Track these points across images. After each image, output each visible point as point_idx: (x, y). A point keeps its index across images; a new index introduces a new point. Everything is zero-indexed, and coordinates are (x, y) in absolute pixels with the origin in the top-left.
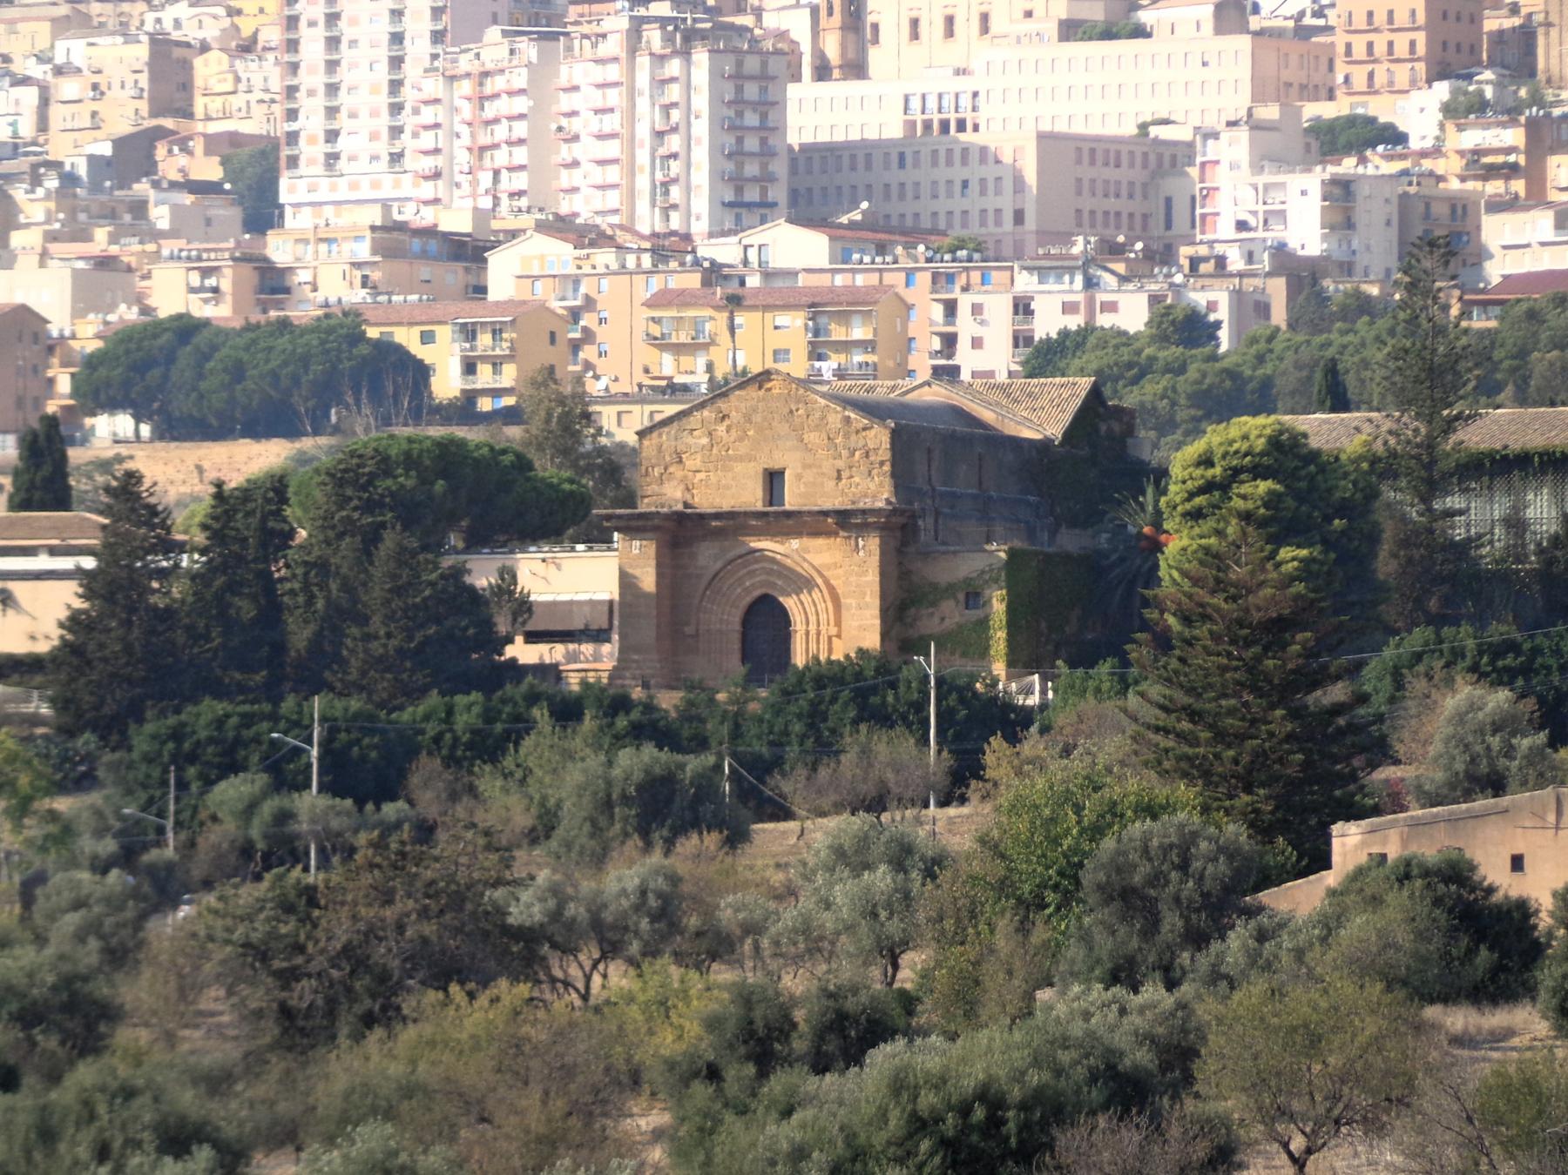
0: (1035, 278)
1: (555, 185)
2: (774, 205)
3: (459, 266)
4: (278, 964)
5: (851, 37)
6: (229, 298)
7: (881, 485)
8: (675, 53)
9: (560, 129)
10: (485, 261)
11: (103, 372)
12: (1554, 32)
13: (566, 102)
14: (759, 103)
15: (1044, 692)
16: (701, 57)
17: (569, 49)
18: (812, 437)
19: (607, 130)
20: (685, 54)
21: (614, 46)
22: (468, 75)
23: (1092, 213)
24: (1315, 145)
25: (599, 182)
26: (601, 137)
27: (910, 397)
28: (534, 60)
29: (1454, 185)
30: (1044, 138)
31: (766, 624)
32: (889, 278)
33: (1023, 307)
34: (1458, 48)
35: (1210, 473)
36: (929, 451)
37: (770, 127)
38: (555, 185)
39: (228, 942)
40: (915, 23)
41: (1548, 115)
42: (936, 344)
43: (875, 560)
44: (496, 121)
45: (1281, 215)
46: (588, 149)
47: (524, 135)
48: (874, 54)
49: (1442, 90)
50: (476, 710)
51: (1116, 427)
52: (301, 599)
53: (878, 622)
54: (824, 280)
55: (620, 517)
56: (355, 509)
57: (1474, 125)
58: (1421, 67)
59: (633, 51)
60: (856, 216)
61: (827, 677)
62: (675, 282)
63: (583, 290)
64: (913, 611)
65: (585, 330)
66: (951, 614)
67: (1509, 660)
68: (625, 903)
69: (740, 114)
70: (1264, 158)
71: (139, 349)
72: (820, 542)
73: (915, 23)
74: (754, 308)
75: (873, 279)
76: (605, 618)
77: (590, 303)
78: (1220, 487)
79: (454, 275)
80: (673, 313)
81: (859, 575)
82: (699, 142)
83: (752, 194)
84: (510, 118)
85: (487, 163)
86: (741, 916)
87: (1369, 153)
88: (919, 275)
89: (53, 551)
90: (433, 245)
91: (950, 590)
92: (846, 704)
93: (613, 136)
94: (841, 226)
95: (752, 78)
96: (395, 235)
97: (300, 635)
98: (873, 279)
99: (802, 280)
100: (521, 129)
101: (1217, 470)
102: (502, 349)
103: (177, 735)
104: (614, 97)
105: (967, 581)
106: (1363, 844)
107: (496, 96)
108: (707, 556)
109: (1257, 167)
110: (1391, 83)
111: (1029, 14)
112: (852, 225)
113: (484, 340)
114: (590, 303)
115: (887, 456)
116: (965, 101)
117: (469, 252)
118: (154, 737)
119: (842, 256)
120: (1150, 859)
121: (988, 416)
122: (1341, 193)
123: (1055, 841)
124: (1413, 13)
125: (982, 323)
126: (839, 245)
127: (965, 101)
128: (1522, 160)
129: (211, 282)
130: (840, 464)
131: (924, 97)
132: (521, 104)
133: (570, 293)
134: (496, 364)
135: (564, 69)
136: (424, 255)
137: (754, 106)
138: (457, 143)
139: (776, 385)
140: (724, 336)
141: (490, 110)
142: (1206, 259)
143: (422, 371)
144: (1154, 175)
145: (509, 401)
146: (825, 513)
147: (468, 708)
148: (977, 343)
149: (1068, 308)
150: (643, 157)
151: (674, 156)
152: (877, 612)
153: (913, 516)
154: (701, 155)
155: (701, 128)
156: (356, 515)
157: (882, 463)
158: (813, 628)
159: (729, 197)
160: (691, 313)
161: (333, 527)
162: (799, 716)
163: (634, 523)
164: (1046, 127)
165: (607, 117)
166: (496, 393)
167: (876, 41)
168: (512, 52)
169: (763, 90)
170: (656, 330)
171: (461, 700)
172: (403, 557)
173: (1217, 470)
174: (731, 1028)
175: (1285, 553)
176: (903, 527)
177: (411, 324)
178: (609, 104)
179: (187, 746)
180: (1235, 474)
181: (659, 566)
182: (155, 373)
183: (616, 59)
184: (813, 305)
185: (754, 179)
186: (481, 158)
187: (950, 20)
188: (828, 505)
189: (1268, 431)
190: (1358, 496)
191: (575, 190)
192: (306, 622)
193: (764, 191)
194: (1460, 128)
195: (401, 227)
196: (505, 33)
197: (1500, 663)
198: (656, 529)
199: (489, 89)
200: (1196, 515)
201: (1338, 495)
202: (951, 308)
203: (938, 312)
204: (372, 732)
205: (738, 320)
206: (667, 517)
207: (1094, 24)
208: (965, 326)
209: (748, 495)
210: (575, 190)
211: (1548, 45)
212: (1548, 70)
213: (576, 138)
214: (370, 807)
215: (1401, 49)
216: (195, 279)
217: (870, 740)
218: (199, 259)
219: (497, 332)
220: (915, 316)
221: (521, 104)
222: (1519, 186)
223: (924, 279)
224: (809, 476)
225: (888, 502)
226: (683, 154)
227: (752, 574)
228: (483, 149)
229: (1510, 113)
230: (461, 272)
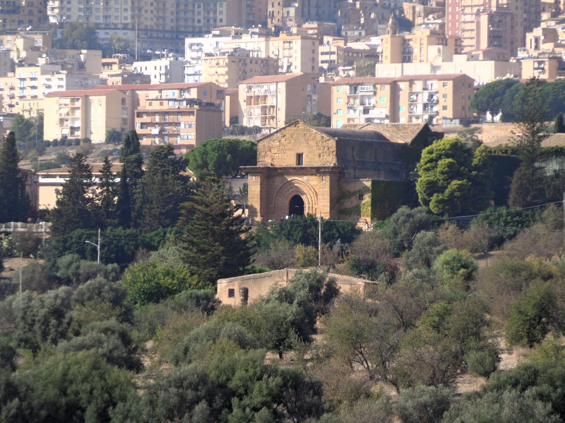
6: (547, 72)
11: (480, 99)
18: (311, 143)
27: (364, 129)
43: (328, 184)
53: (329, 204)
55: (248, 168)
64: (343, 200)
67: (517, 218)
71: (493, 90)
81: (323, 188)
91: (354, 194)
101: (434, 155)
105: (359, 191)
106: (227, 286)
108: (278, 182)
115: (335, 149)
120: (90, 292)
121: (387, 135)
129: (542, 66)
130: (320, 152)
146: (312, 168)
152: (329, 201)
157: (333, 152)
158: (311, 206)
163: (253, 171)
173: (434, 155)
176: (340, 173)
179: (68, 244)
181: (261, 185)
182: (498, 99)
188: (316, 165)
197: (514, 219)
198: (260, 173)
200: (427, 170)
201: (473, 164)
209: (291, 162)
216: (536, 65)
218: (538, 58)
224: (310, 155)
225: (335, 164)
227: (292, 187)
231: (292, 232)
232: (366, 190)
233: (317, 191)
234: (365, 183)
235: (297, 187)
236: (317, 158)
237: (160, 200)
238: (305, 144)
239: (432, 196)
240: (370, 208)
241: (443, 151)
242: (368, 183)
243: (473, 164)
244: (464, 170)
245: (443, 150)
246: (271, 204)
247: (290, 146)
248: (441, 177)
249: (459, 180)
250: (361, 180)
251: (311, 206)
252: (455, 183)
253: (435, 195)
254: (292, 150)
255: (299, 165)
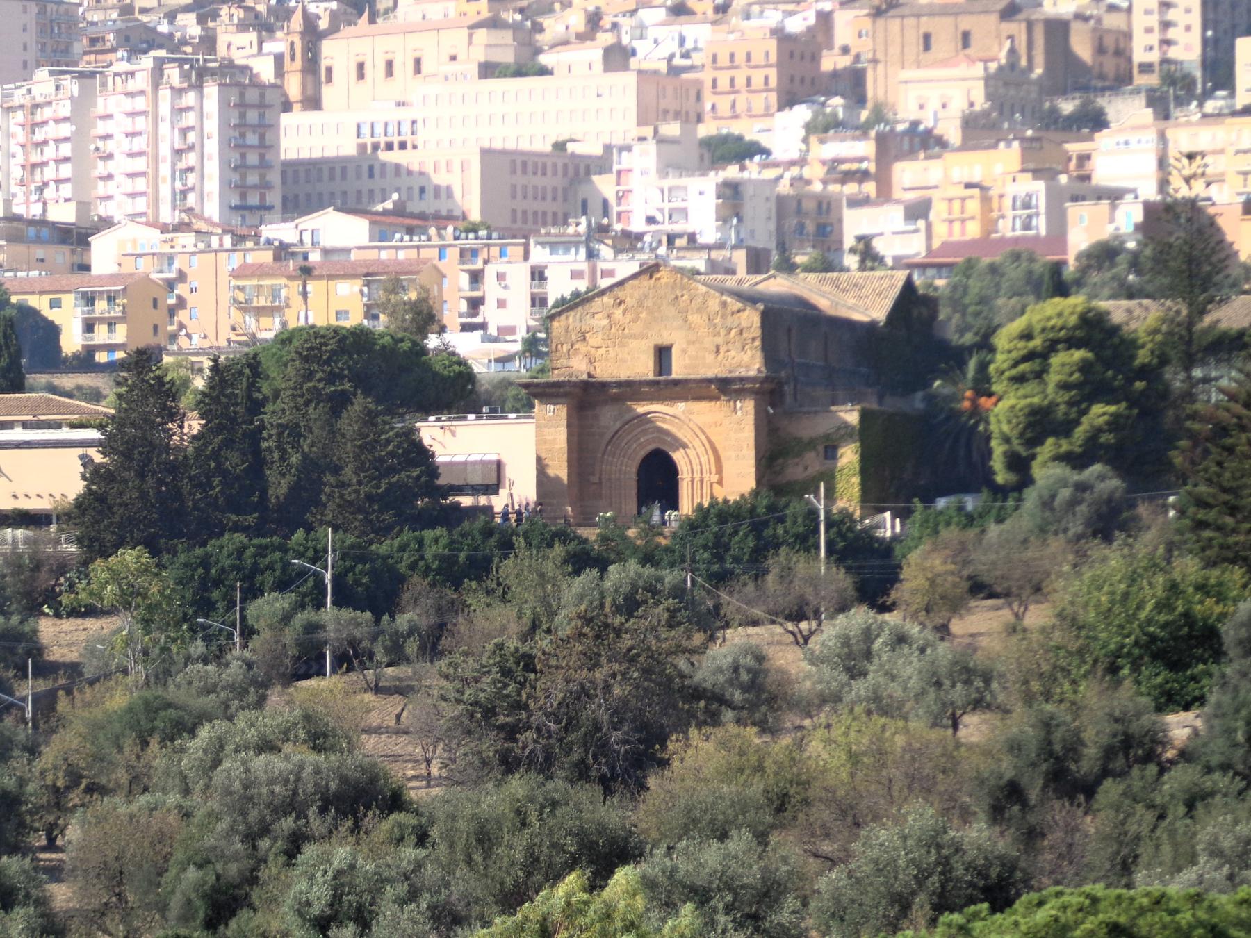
0: (547, 250)
1: (94, 194)
2: (270, 208)
3: (66, 249)
4: (502, 719)
5: (310, 78)
7: (753, 357)
8: (191, 87)
9: (97, 149)
10: (88, 244)
12: (880, 67)
13: (102, 128)
14: (260, 126)
15: (893, 527)
16: (212, 90)
17: (104, 84)
18: (694, 318)
19: (136, 149)
20: (199, 87)
21: (142, 81)
22: (22, 107)
23: (525, 212)
24: (707, 156)
25: (130, 190)
26: (131, 155)
27: (760, 287)
28: (76, 94)
29: (817, 187)
30: (486, 153)
31: (659, 477)
32: (425, 253)
33: (538, 275)
34: (802, 80)
35: (1031, 344)
36: (789, 330)
37: (267, 145)
38: (94, 194)
39: (458, 701)
40: (361, 66)
41: (892, 130)
42: (464, 306)
43: (749, 420)
44: (45, 143)
45: (684, 212)
46: (120, 165)
47: (69, 154)
48: (327, 92)
49: (802, 113)
50: (443, 541)
51: (925, 311)
52: (276, 455)
54: (371, 255)
56: (320, 380)
57: (834, 139)
58: (773, 98)
59: (156, 86)
60: (389, 205)
61: (720, 516)
62: (251, 258)
63: (176, 265)
64: (780, 461)
65: (179, 298)
66: (812, 462)
68: (721, 678)
69: (243, 135)
70: (667, 166)
72: (704, 405)
73: (361, 66)
74: (320, 277)
75: (413, 254)
76: (494, 474)
77: (182, 276)
78: (1041, 356)
79: (61, 255)
80: (254, 282)
82: (210, 158)
83: (254, 200)
84: (56, 141)
85: (38, 177)
86: (819, 687)
87: (747, 162)
88: (449, 250)
89: (26, 425)
90: (45, 232)
91: (811, 444)
92: (746, 535)
93: (140, 154)
94: (377, 213)
95: (252, 106)
96: (15, 224)
97: (279, 486)
98: (413, 254)
99: (354, 256)
100: (66, 150)
102: (117, 312)
103: (205, 563)
104: (141, 123)
105: (827, 437)
107: (45, 123)
108: (608, 418)
109: (663, 172)
110: (749, 109)
111: (453, 58)
112: (385, 213)
113: (101, 306)
114: (182, 276)
116: (406, 128)
117: (76, 237)
118: (186, 565)
119: (381, 233)
122: (732, 194)
123: (1132, 618)
124: (767, 54)
125: (506, 287)
126: (377, 229)
127: (406, 128)
128: (872, 167)
130: (719, 340)
131: (386, 125)
132: (66, 130)
133: (166, 267)
134: (111, 323)
135: (100, 101)
136: (38, 240)
137: (254, 128)
138: (13, 161)
139: (663, 273)
140: (297, 300)
141: (39, 136)
142: (680, 236)
143: (52, 331)
144: (572, 182)
145: (120, 355)
146: (709, 381)
147: (435, 540)
148: (501, 304)
149: (575, 275)
150: (165, 170)
151: (191, 169)
152: (752, 462)
153: (780, 384)
154: (213, 168)
155: (212, 147)
156: (321, 385)
157: (754, 339)
158: (697, 476)
159: (235, 201)
160: (267, 282)
161: (302, 396)
162: (705, 547)
164: (486, 145)
165: (136, 139)
166: (111, 348)
167: (329, 79)
168: (58, 88)
169: (262, 116)
170: (241, 297)
171: (428, 534)
172: (370, 418)
174: (1032, 749)
175: (1097, 409)
176: (772, 392)
177: (41, 293)
178: (138, 129)
180: (1052, 346)
181: (569, 426)
183: (142, 93)
184: (367, 275)
185: (255, 187)
186: (32, 173)
187: (389, 65)
188: (710, 374)
189: (1079, 309)
190: (1155, 361)
191: (109, 198)
192: (283, 475)
193: (263, 197)
194: (822, 141)
195: (18, 218)
196: (51, 73)
198: (565, 395)
199: (38, 118)
200: (1020, 379)
201: (1137, 362)
202: (476, 277)
203: (464, 279)
204: (363, 559)
205: (309, 288)
206: (575, 384)
207: (507, 66)
208: (490, 289)
209: (642, 367)
210: (109, 198)
211: (875, 81)
212: (875, 94)
213: (110, 156)
214: (386, 618)
215: (758, 82)
217: (789, 560)
219: (111, 299)
220: (446, 284)
221: (66, 130)
222: (870, 188)
223: (453, 254)
224: (692, 350)
225: (759, 371)
226: (198, 168)
227: (645, 432)
228: (34, 166)
229: (862, 131)
230: (68, 253)
231: (726, 539)
232: (846, 433)
233: (713, 439)
234: (842, 414)
235: (660, 430)
236: (710, 358)
237: (363, 463)
238: (679, 322)
239: (1042, 443)
240: (856, 480)
241: (1063, 333)
242: (851, 416)
243: (1137, 362)
244: (1114, 378)
245: (1062, 329)
246: (593, 474)
247: (637, 328)
248: (1064, 397)
249: (1108, 403)
250: (833, 408)
251: (697, 476)
252: (1100, 413)
253: (1050, 441)
254: (643, 336)
255: (660, 374)
